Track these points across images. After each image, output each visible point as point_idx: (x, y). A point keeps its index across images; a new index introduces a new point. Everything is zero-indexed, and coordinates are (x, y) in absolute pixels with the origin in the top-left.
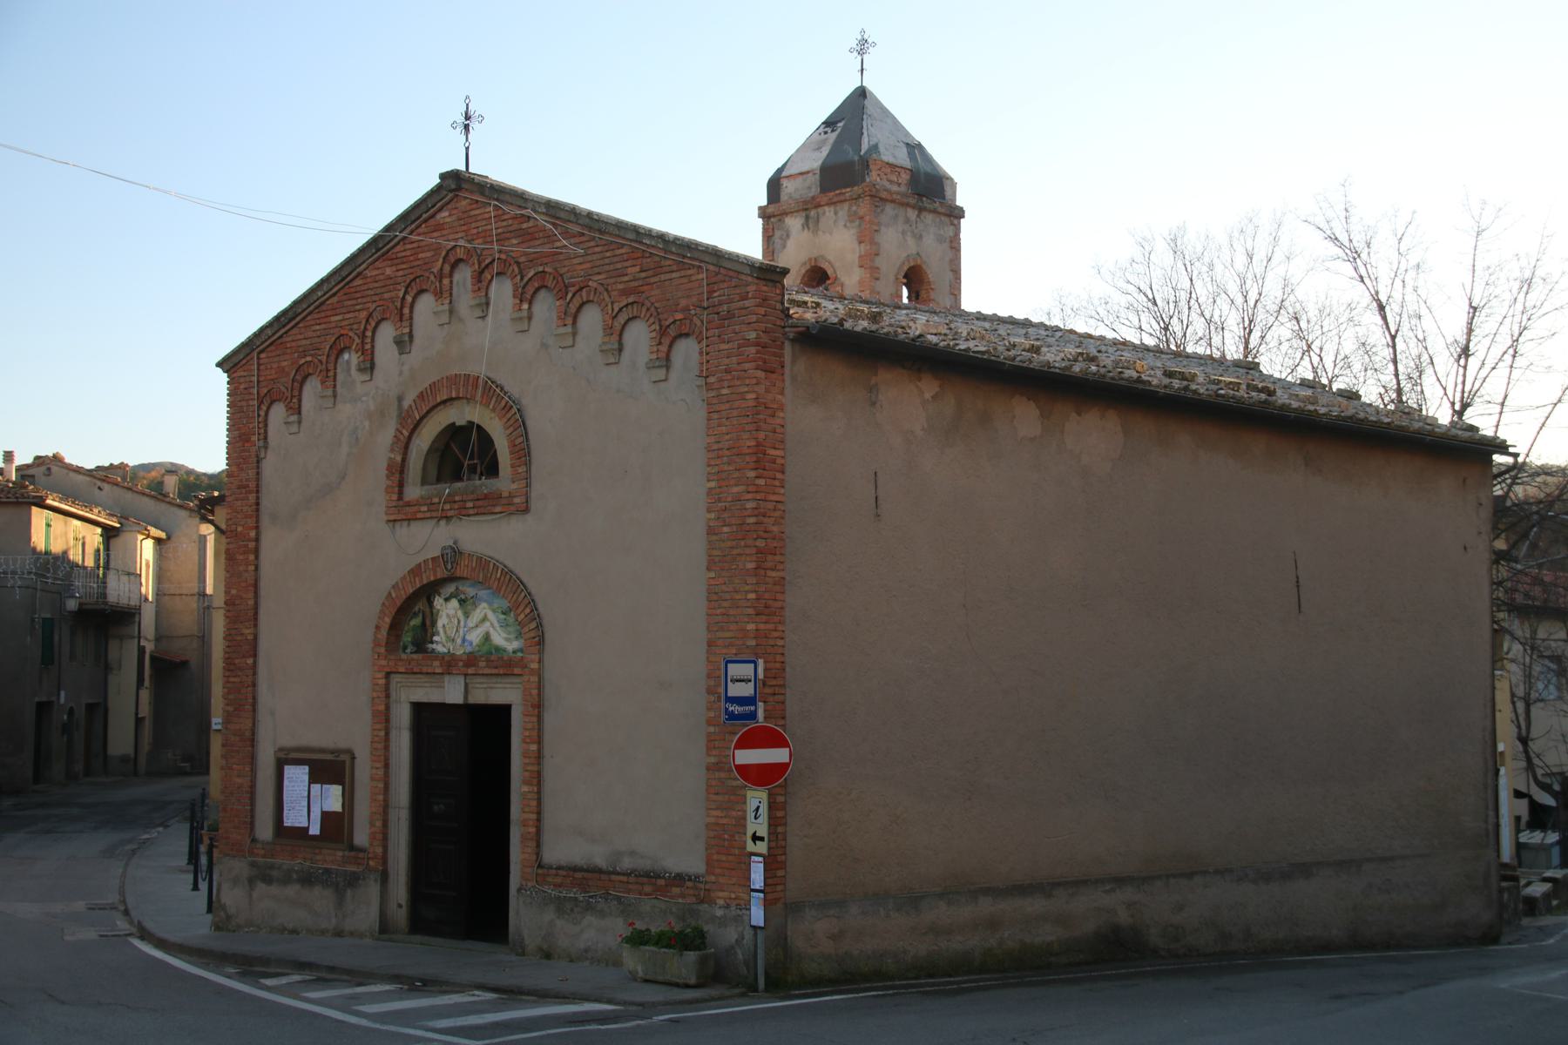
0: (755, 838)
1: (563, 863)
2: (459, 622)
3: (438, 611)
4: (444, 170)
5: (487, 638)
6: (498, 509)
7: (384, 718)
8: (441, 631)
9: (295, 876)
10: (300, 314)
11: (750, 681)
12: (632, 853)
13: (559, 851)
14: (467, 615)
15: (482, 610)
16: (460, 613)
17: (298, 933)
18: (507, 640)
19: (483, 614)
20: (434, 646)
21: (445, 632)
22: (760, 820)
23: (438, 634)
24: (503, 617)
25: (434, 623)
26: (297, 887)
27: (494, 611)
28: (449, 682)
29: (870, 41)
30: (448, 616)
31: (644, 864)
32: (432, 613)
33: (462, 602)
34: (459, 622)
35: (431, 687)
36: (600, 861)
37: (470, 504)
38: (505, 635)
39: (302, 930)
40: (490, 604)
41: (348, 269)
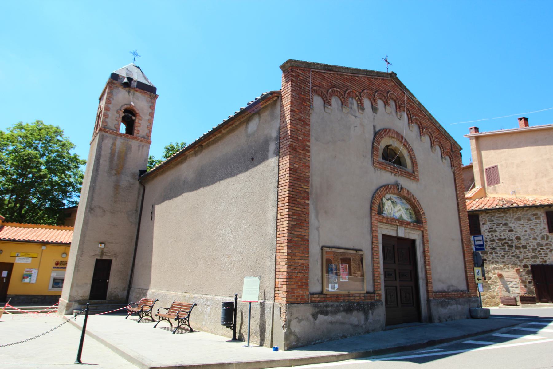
0: (478, 279)
1: (437, 290)
2: (392, 209)
3: (385, 203)
4: (394, 72)
5: (401, 216)
6: (412, 178)
7: (373, 238)
8: (386, 210)
9: (341, 309)
10: (334, 71)
11: (481, 241)
12: (452, 286)
13: (437, 286)
14: (394, 207)
15: (398, 207)
16: (392, 206)
17: (346, 337)
18: (408, 218)
19: (399, 209)
20: (384, 215)
21: (387, 211)
22: (479, 275)
23: (385, 211)
24: (405, 211)
25: (383, 207)
26: (344, 314)
27: (403, 208)
28: (399, 229)
29: (134, 51)
30: (388, 205)
31: (455, 288)
32: (382, 203)
33: (393, 202)
34: (392, 209)
35: (390, 229)
36: (445, 289)
37: (404, 173)
38: (407, 217)
39: (348, 335)
40: (401, 206)
41: (356, 72)
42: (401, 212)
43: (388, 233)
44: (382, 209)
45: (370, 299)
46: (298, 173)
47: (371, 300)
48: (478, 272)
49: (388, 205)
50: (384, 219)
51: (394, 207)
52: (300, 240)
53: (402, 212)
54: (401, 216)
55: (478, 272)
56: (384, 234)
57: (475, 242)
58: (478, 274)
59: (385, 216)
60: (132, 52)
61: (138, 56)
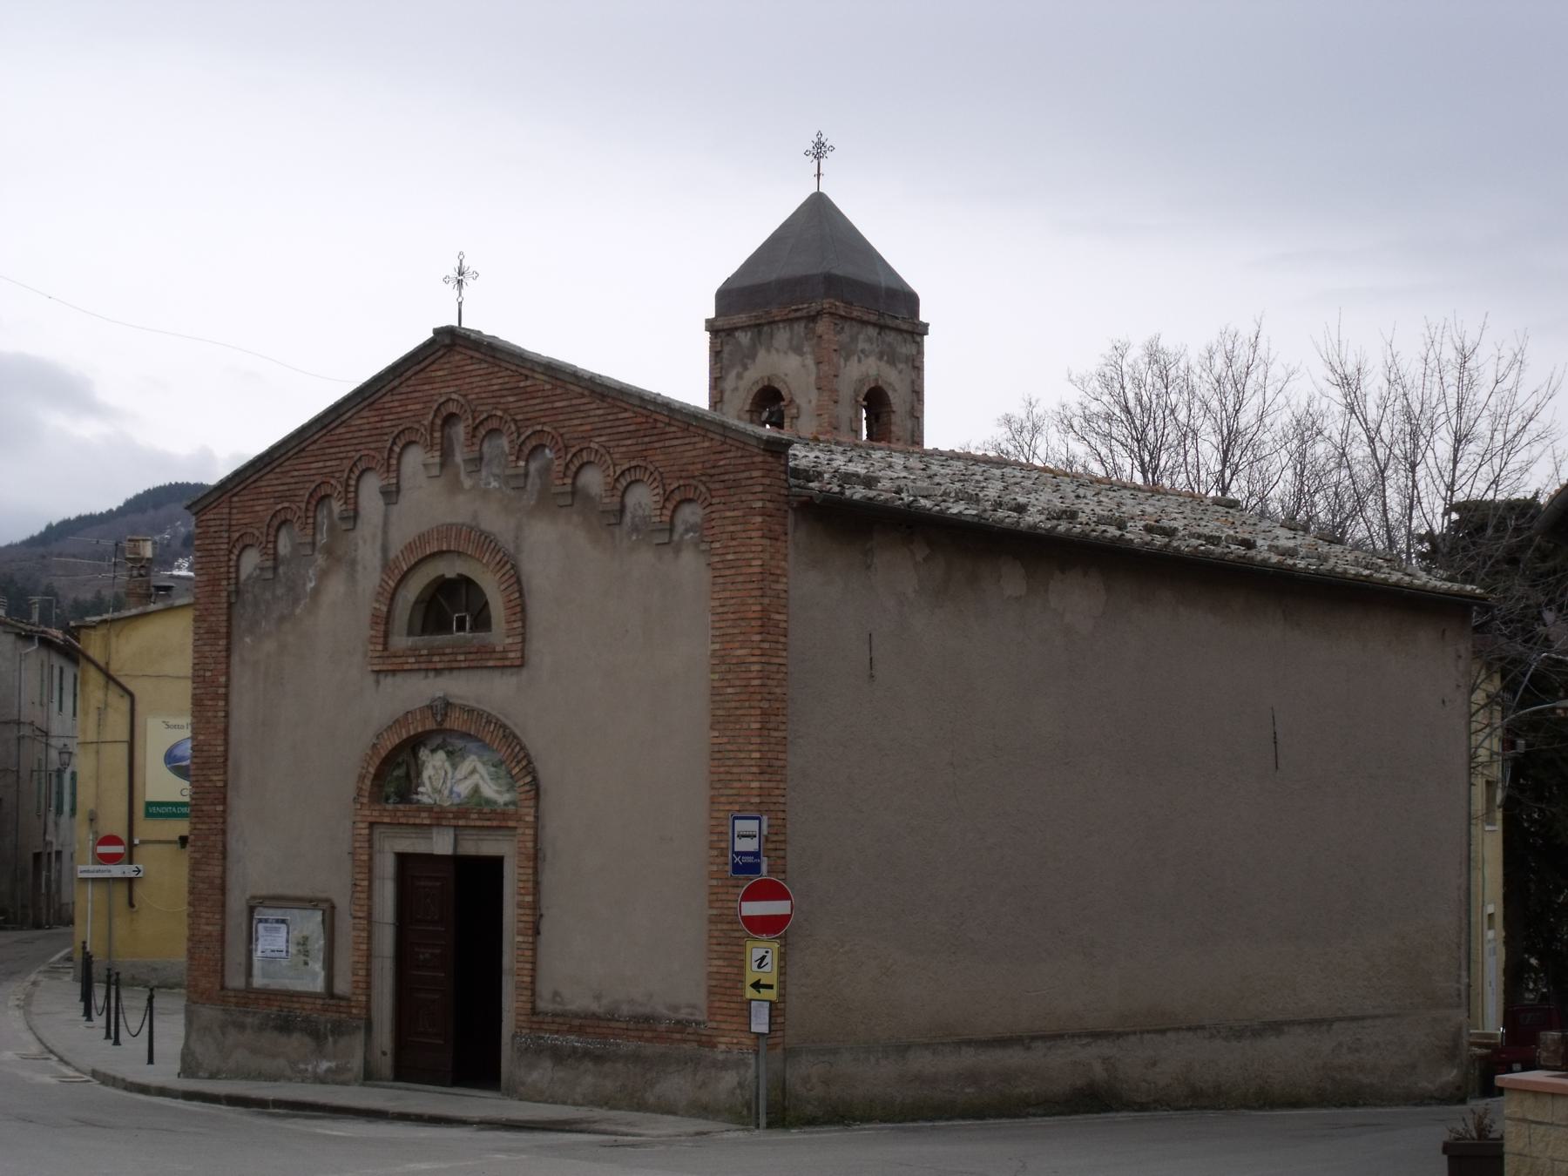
2: (446, 773)
3: (424, 762)
5: (476, 790)
8: (427, 782)
11: (755, 836)
16: (447, 765)
19: (471, 767)
20: (419, 797)
22: (767, 969)
24: (493, 769)
27: (484, 764)
30: (434, 767)
38: (495, 788)
40: (480, 757)
41: (333, 416)
42: (476, 777)
43: (410, 850)
44: (414, 782)
45: (336, 1012)
46: (206, 751)
47: (338, 1015)
48: (763, 958)
49: (434, 767)
50: (386, 814)
51: (455, 766)
52: (206, 886)
53: (482, 777)
54: (476, 790)
55: (763, 958)
56: (401, 851)
57: (736, 839)
58: (759, 967)
59: (425, 799)
60: (823, 140)
61: (816, 161)
